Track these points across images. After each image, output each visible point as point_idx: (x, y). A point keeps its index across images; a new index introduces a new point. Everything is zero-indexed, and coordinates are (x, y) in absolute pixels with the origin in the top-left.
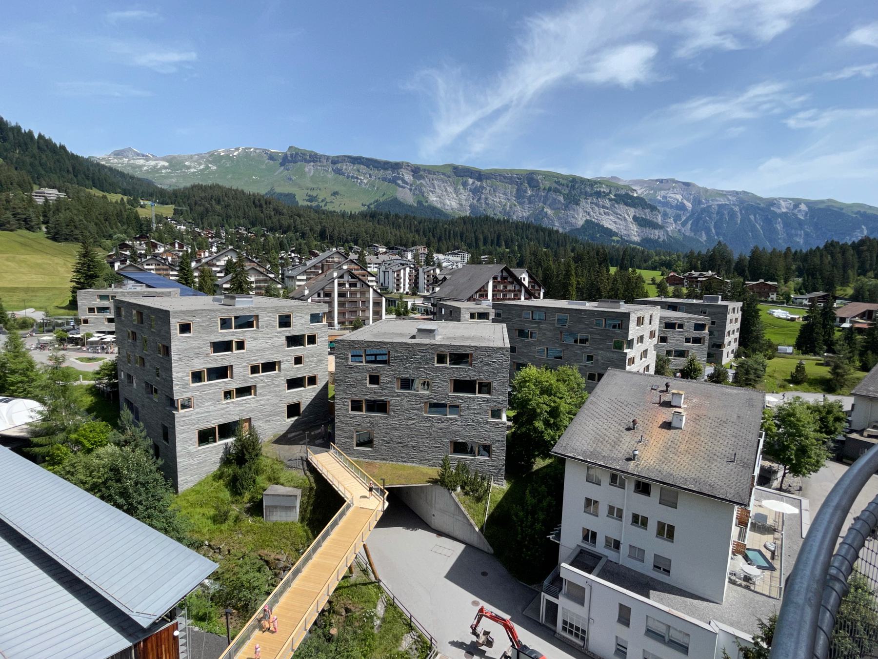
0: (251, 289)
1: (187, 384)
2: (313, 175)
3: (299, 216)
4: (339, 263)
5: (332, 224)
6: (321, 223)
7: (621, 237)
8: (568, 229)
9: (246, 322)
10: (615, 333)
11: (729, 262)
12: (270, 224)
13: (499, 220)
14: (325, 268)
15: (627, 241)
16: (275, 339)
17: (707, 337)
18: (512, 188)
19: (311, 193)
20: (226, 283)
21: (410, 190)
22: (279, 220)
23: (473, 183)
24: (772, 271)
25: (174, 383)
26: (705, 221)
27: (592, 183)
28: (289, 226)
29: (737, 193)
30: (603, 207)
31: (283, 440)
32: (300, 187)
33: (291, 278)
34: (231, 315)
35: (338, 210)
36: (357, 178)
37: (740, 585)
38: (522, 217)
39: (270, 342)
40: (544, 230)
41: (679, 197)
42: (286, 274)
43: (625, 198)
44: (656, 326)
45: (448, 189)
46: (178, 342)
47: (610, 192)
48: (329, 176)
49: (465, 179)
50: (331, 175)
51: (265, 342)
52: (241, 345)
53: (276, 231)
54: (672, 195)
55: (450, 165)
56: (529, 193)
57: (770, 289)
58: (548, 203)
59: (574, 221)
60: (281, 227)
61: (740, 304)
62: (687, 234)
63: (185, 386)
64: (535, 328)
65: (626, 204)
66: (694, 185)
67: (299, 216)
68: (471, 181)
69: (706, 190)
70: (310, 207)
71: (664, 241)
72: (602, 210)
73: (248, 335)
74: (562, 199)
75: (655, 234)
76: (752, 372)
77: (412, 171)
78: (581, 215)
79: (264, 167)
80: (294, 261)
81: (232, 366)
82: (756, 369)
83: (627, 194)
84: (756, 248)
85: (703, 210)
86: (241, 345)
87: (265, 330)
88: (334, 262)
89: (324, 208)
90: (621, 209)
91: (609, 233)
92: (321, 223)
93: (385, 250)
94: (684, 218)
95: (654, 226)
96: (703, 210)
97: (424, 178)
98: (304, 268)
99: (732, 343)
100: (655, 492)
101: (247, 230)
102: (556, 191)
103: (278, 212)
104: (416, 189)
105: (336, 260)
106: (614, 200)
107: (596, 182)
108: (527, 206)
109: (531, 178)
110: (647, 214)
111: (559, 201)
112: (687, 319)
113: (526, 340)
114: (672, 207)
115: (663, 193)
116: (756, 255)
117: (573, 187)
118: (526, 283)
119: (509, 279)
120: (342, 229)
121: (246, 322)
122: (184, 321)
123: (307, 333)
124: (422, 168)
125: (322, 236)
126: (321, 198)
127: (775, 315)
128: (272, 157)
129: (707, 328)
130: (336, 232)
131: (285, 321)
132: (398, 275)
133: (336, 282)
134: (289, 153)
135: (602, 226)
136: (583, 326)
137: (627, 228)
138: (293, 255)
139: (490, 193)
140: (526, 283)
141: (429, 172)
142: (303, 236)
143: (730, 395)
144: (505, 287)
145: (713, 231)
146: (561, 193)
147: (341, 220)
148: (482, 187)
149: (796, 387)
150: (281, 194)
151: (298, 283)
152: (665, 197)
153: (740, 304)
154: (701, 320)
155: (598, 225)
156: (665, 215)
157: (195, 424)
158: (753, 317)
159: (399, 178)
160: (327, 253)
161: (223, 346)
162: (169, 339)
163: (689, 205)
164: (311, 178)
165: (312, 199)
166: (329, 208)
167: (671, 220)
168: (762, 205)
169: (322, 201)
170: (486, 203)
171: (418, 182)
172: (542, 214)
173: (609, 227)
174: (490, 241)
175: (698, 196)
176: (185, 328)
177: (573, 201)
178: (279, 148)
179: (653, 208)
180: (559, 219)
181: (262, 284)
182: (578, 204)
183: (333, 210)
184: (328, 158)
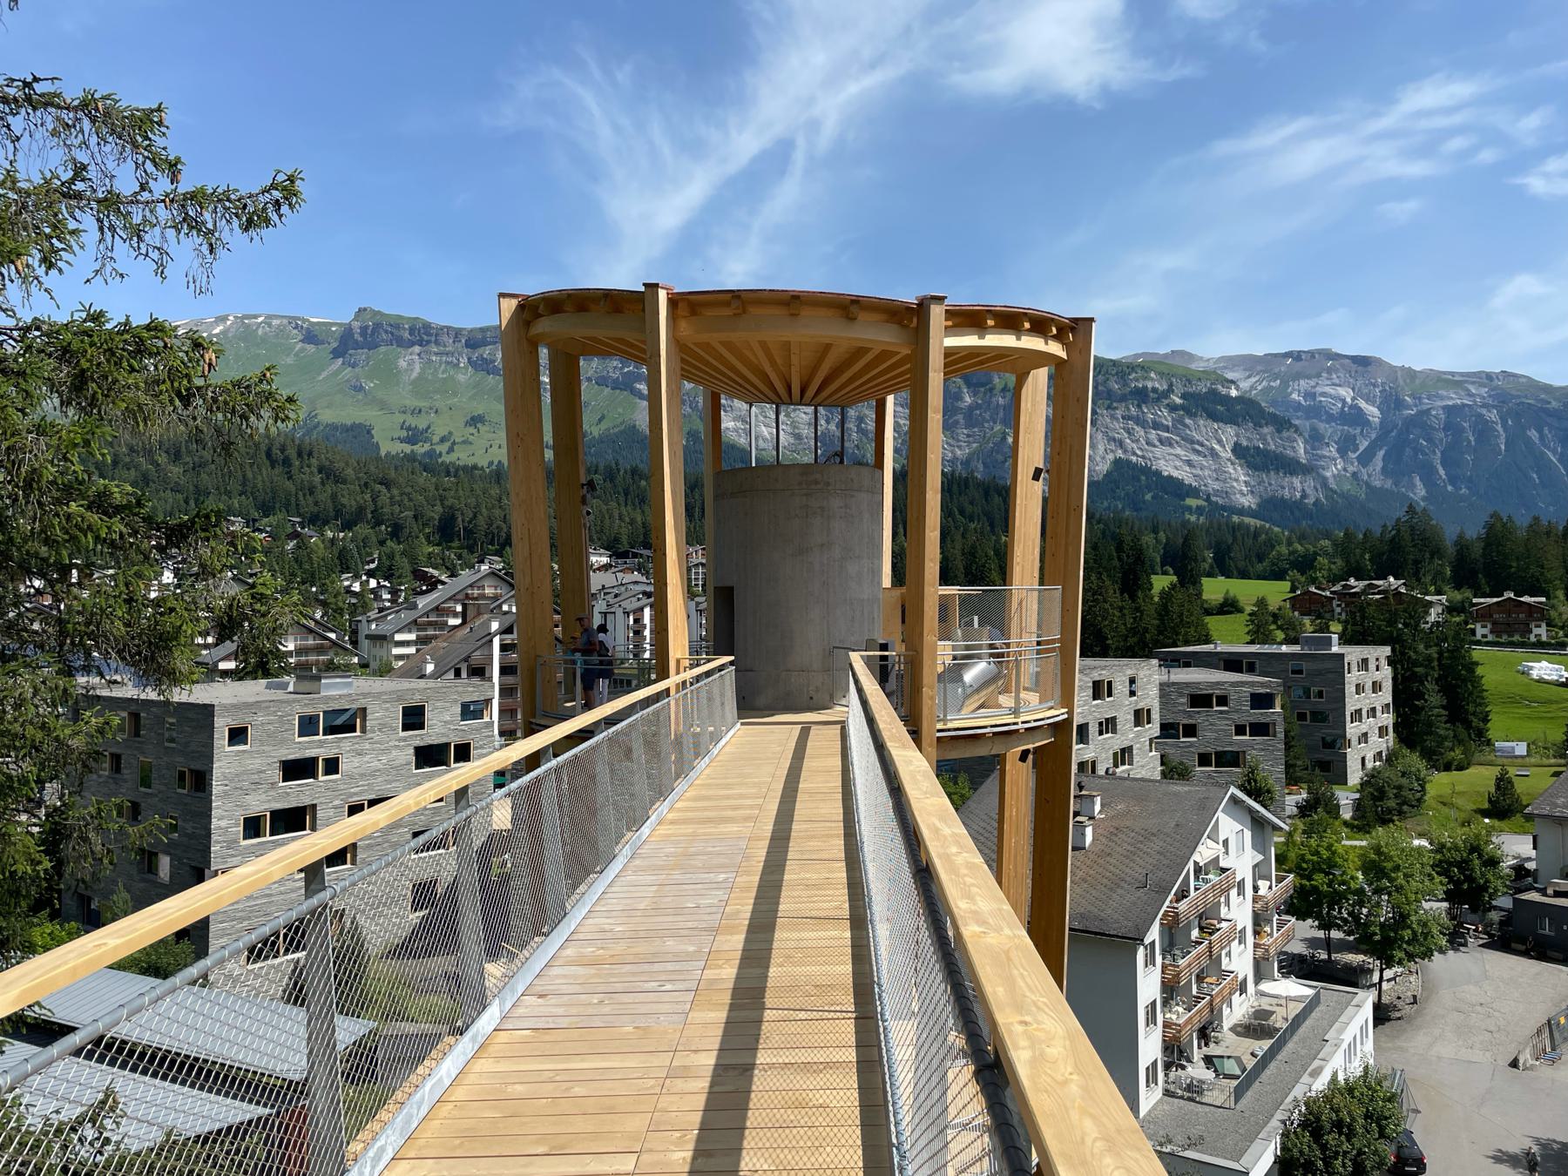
0: (285, 670)
1: (236, 841)
2: (420, 377)
3: (386, 483)
4: (496, 598)
5: (472, 501)
6: (442, 499)
7: (1208, 499)
9: (344, 723)
11: (1437, 552)
12: (308, 506)
14: (470, 613)
15: (1224, 508)
16: (394, 753)
17: (1280, 719)
19: (412, 421)
20: (226, 658)
22: (334, 497)
24: (1534, 569)
25: (214, 838)
26: (1417, 450)
28: (361, 510)
29: (1489, 376)
30: (1157, 426)
31: (403, 950)
32: (383, 405)
33: (381, 639)
34: (319, 710)
35: (483, 462)
37: (1182, 1097)
39: (384, 759)
41: (1346, 393)
42: (364, 630)
43: (1206, 399)
44: (1150, 697)
46: (226, 761)
47: (1170, 390)
48: (461, 378)
50: (465, 376)
51: (378, 752)
52: (332, 766)
53: (326, 522)
54: (1328, 389)
56: (968, 399)
57: (1530, 615)
60: (338, 513)
61: (1387, 650)
62: (1377, 484)
63: (232, 844)
65: (1214, 417)
66: (1379, 362)
67: (386, 483)
69: (1410, 373)
70: (411, 458)
71: (1317, 503)
72: (1153, 435)
73: (346, 746)
75: (1294, 487)
76: (1391, 793)
80: (378, 598)
81: (314, 806)
82: (1400, 788)
83: (1213, 393)
84: (1495, 515)
85: (1413, 418)
86: (332, 766)
87: (377, 736)
88: (483, 597)
89: (447, 459)
90: (1202, 429)
91: (1177, 489)
92: (442, 499)
93: (605, 560)
94: (1364, 445)
95: (1290, 467)
96: (1411, 423)
98: (413, 615)
99: (1374, 738)
101: (250, 522)
103: (330, 474)
105: (489, 591)
106: (1182, 407)
108: (962, 432)
110: (1268, 439)
112: (1234, 684)
114: (1331, 418)
115: (1304, 384)
116: (1496, 535)
120: (497, 512)
121: (344, 723)
122: (235, 724)
123: (455, 740)
125: (446, 531)
126: (439, 431)
127: (1535, 674)
128: (311, 336)
129: (1278, 702)
130: (481, 521)
131: (414, 718)
132: (636, 621)
133: (496, 641)
134: (356, 324)
135: (1158, 473)
137: (1220, 475)
138: (373, 583)
142: (396, 532)
143: (1176, 794)
145: (1442, 472)
147: (495, 491)
149: (1497, 823)
150: (334, 427)
151: (396, 651)
152: (1309, 395)
153: (1387, 650)
154: (1262, 685)
155: (1146, 470)
156: (1315, 439)
157: (242, 919)
158: (1464, 681)
160: (466, 577)
161: (297, 769)
162: (209, 758)
163: (1372, 411)
164: (414, 383)
165: (414, 436)
166: (461, 457)
167: (1333, 451)
168: (1554, 404)
169: (443, 440)
173: (1175, 474)
175: (1397, 388)
176: (238, 735)
178: (335, 313)
179: (1281, 424)
181: (312, 658)
183: (470, 462)
184: (457, 333)
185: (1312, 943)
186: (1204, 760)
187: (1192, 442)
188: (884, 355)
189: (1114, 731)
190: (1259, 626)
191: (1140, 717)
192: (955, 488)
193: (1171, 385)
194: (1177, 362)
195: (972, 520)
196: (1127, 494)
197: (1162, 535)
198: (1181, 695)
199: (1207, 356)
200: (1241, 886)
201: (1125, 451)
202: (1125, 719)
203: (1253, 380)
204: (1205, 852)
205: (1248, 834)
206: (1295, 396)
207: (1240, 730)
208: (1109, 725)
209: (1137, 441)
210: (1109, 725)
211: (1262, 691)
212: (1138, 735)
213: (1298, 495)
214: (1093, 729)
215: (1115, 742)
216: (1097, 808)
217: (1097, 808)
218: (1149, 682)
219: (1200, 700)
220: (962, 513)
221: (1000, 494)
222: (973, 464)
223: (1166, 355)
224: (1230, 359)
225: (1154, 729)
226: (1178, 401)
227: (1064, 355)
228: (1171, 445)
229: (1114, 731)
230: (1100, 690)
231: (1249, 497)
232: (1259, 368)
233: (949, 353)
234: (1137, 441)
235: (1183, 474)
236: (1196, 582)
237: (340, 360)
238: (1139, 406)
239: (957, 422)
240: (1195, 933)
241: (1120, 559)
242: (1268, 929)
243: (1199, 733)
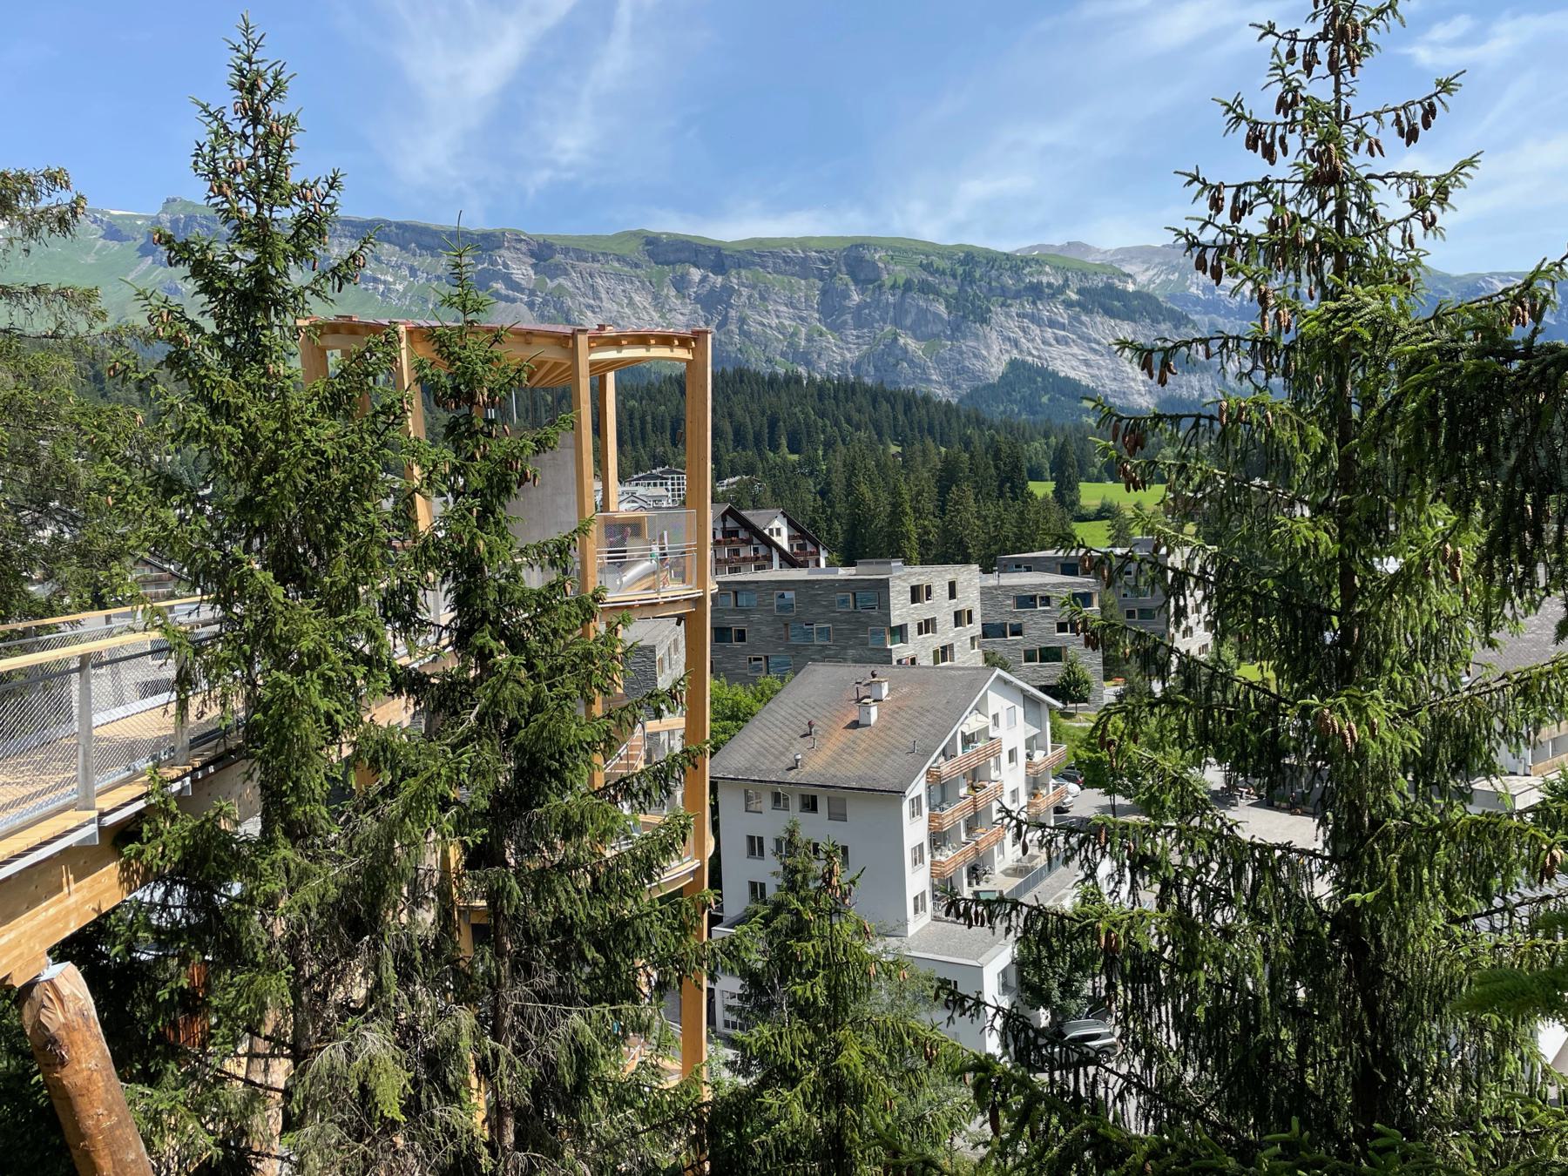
8: (965, 387)
10: (870, 617)
13: (773, 380)
18: (810, 287)
21: (531, 305)
23: (704, 279)
27: (1017, 264)
30: (1053, 324)
36: (375, 280)
38: (842, 365)
40: (891, 398)
44: (970, 599)
45: (637, 298)
47: (1066, 285)
49: (679, 269)
55: (635, 234)
56: (856, 298)
58: (908, 322)
59: (978, 364)
64: (742, 621)
65: (1110, 313)
68: (696, 274)
72: (1049, 333)
74: (941, 309)
77: (532, 254)
78: (996, 348)
79: (91, 260)
83: (1110, 288)
91: (1072, 390)
97: (566, 274)
100: (822, 805)
102: (925, 288)
104: (545, 303)
106: (1079, 304)
107: (1027, 261)
108: (851, 333)
109: (855, 260)
111: (937, 316)
112: (1054, 585)
113: (728, 645)
117: (968, 278)
118: (783, 541)
119: (743, 534)
124: (558, 244)
129: (1096, 600)
134: (165, 218)
135: (1054, 374)
136: (820, 610)
139: (753, 307)
140: (783, 541)
141: (580, 255)
144: (736, 552)
146: (938, 293)
148: (728, 291)
154: (1081, 585)
155: (1043, 372)
159: (496, 276)
170: (743, 333)
171: (551, 284)
172: (891, 354)
173: (1072, 374)
174: (750, 437)
177: (971, 312)
180: (940, 361)
182: (984, 321)
185: (1104, 809)
186: (1029, 657)
187: (1089, 340)
188: (556, 365)
189: (934, 631)
190: (1119, 531)
191: (960, 618)
192: (841, 395)
193: (1067, 280)
194: (1073, 255)
195: (858, 428)
196: (1023, 397)
197: (1053, 440)
198: (1008, 597)
199: (1105, 247)
200: (1012, 755)
201: (1021, 352)
202: (945, 619)
203: (1151, 273)
204: (972, 723)
205: (1020, 711)
206: (1193, 290)
207: (1062, 627)
208: (927, 626)
209: (1033, 340)
210: (927, 626)
211: (1081, 590)
212: (959, 634)
213: (1196, 394)
214: (912, 630)
215: (935, 641)
216: (885, 691)
217: (885, 691)
218: (969, 586)
219: (1026, 601)
220: (849, 421)
221: (888, 401)
222: (864, 367)
223: (1062, 248)
224: (1127, 251)
225: (976, 629)
226: (1074, 297)
227: (690, 357)
228: (1067, 344)
229: (934, 631)
230: (916, 594)
231: (1147, 397)
232: (1157, 260)
233: (592, 364)
234: (1033, 340)
235: (1081, 375)
236: (1073, 488)
237: (150, 259)
238: (1034, 303)
239: (845, 322)
240: (963, 791)
241: (997, 467)
242: (1044, 792)
243: (1025, 632)
